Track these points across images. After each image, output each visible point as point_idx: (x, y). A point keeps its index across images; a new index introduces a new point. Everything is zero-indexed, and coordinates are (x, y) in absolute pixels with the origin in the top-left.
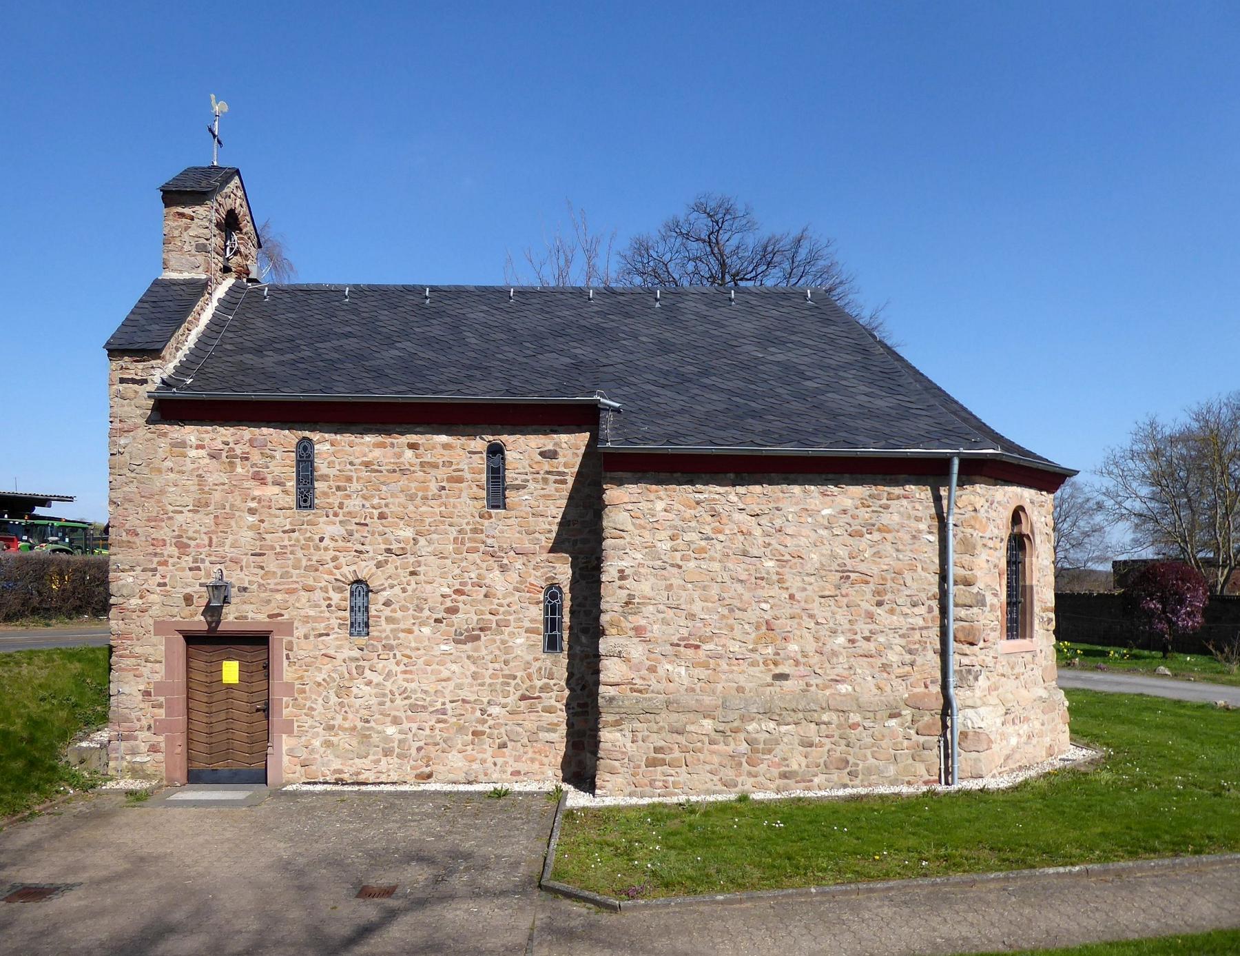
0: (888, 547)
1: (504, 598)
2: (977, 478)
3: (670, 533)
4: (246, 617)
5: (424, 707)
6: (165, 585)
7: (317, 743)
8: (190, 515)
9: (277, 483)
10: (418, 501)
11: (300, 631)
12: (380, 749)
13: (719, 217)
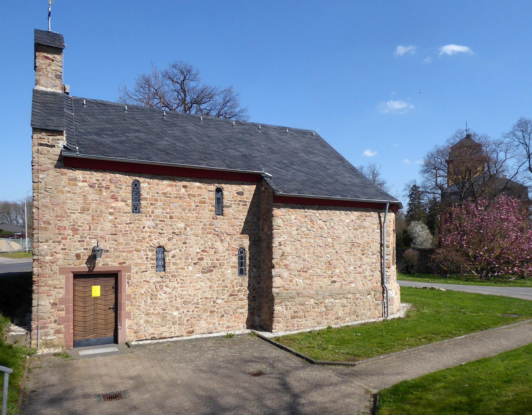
0: (366, 234)
1: (222, 253)
4: (108, 264)
5: (189, 302)
6: (65, 249)
7: (142, 322)
8: (79, 215)
9: (123, 201)
10: (187, 211)
11: (134, 270)
12: (171, 322)
13: (186, 73)
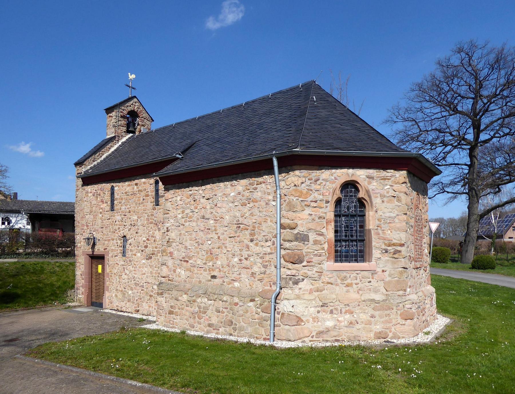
2: (295, 167)
3: (181, 210)
